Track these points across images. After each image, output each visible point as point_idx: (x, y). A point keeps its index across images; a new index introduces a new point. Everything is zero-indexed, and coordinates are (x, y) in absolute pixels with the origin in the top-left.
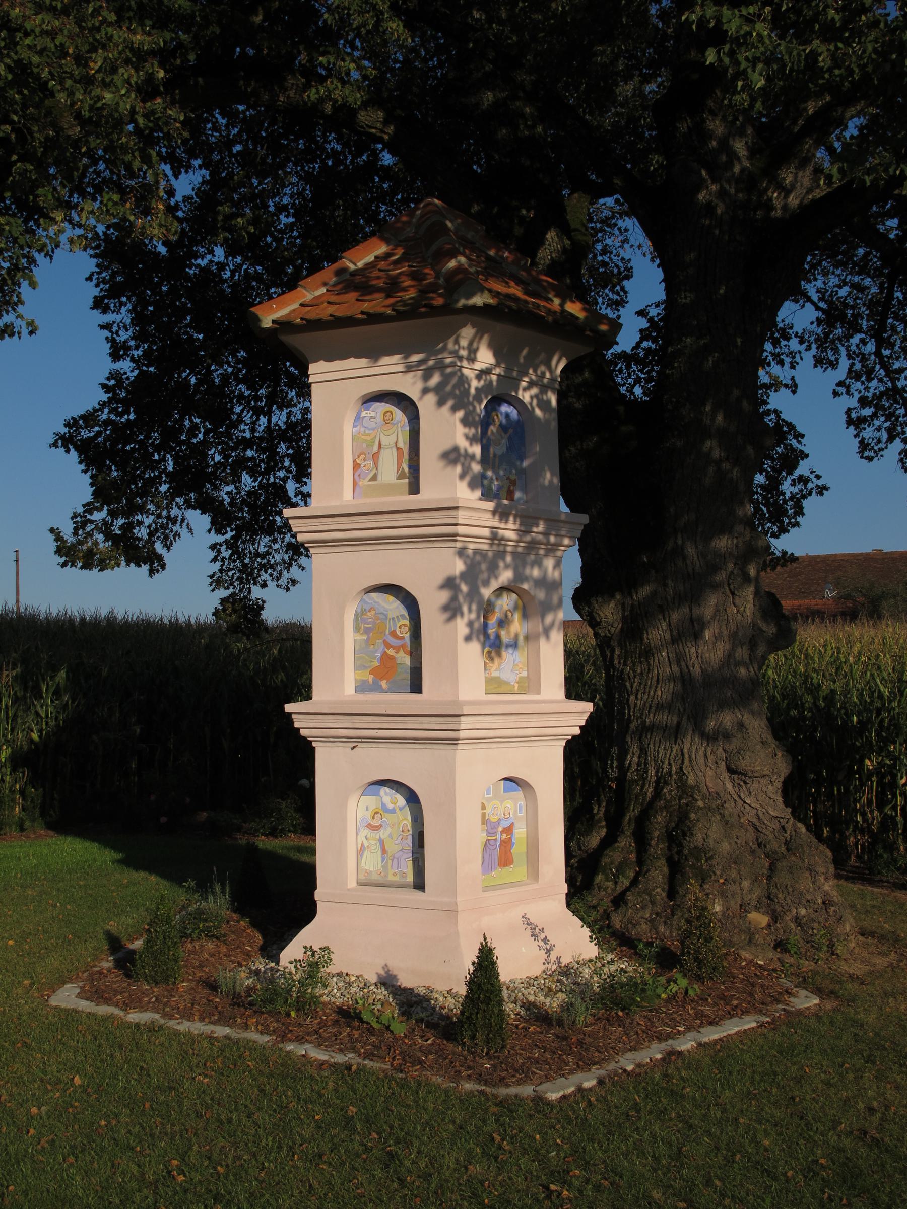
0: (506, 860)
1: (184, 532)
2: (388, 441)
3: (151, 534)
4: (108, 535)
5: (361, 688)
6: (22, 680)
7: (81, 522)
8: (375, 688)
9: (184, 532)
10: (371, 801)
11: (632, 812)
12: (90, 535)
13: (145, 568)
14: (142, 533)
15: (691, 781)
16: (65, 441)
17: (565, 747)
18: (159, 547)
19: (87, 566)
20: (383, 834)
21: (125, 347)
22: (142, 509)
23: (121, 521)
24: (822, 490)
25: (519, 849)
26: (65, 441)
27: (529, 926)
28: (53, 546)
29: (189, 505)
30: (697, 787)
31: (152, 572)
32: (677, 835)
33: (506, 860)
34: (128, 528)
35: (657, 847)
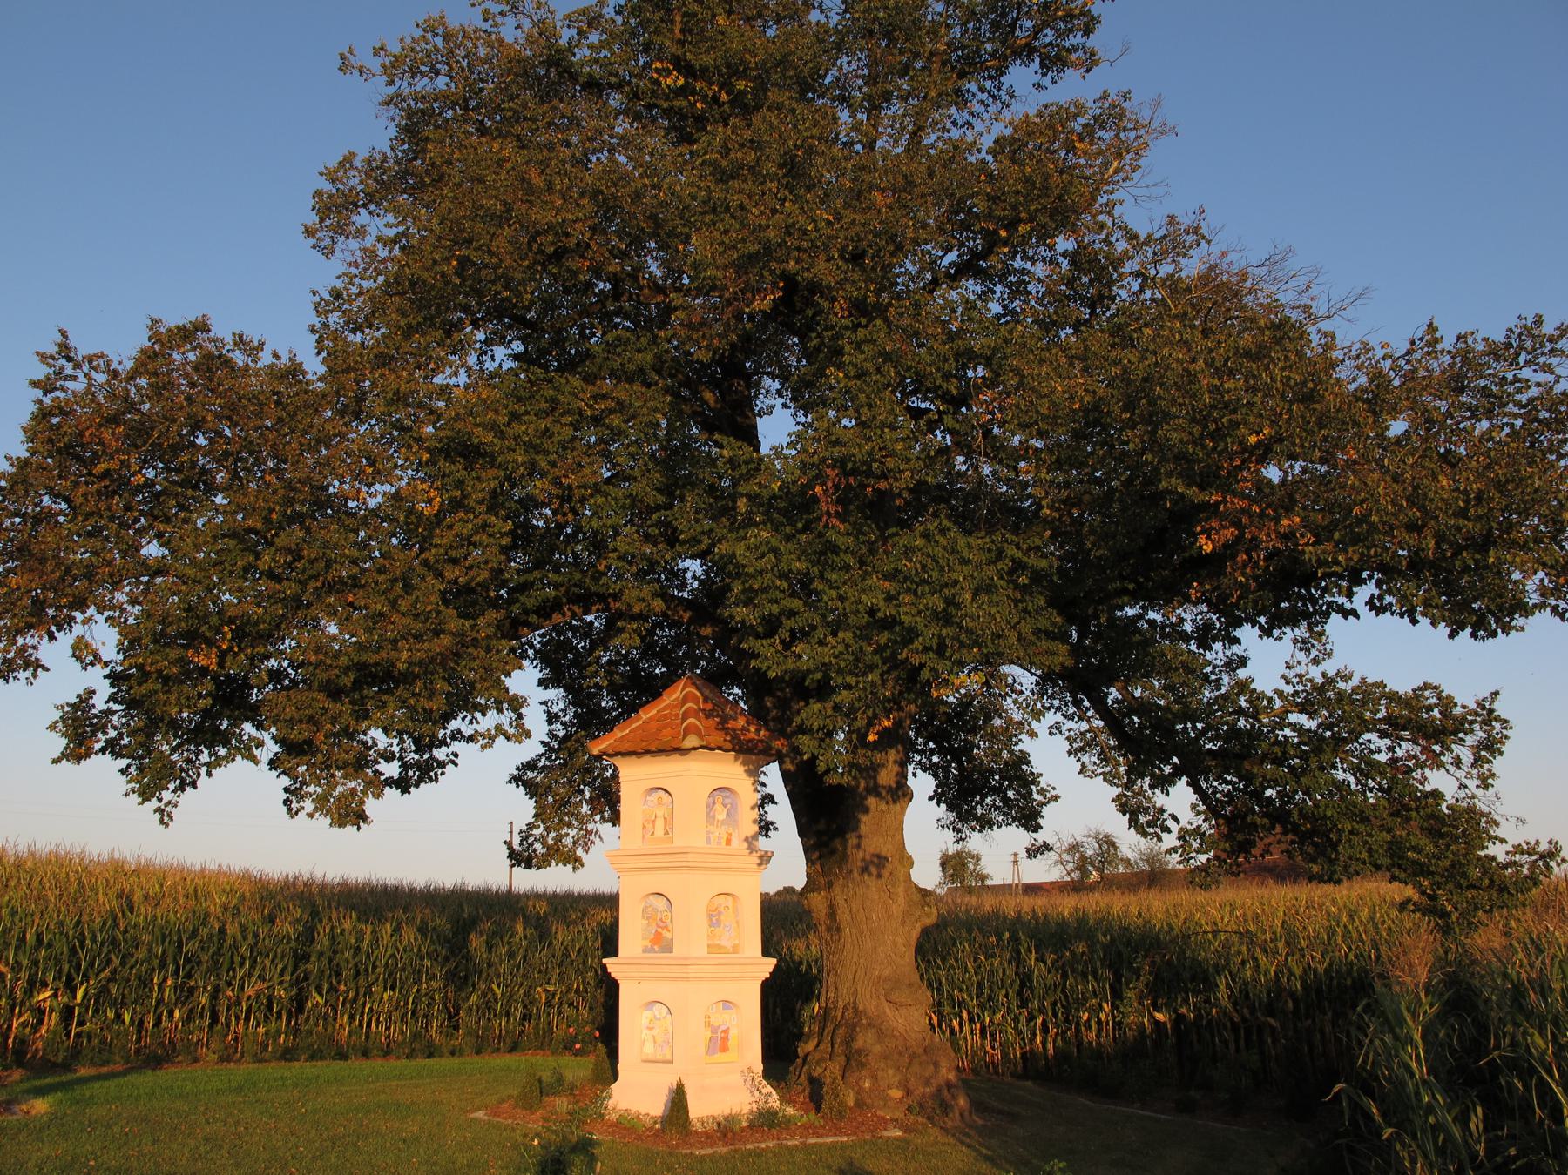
0: (724, 1048)
1: (597, 840)
2: (660, 814)
3: (575, 843)
4: (544, 844)
5: (645, 950)
6: (1247, 993)
7: (526, 835)
8: (652, 950)
9: (597, 840)
10: (648, 1014)
11: (830, 1027)
12: (531, 844)
13: (570, 867)
14: (568, 841)
15: (861, 1008)
16: (516, 780)
17: (766, 985)
18: (580, 852)
19: (529, 866)
20: (655, 1032)
21: (557, 717)
22: (569, 825)
23: (553, 834)
24: (1055, 798)
25: (732, 1043)
26: (516, 780)
27: (730, 1085)
28: (507, 852)
29: (603, 819)
30: (864, 1012)
31: (574, 868)
32: (849, 1041)
33: (724, 1048)
34: (558, 839)
35: (838, 1049)
